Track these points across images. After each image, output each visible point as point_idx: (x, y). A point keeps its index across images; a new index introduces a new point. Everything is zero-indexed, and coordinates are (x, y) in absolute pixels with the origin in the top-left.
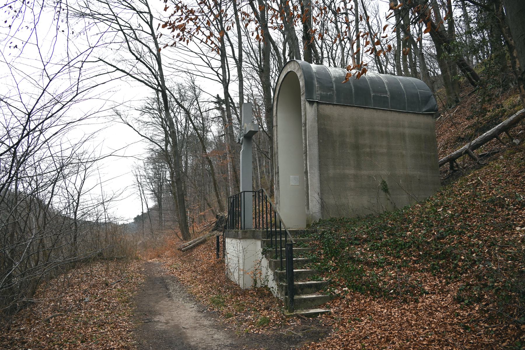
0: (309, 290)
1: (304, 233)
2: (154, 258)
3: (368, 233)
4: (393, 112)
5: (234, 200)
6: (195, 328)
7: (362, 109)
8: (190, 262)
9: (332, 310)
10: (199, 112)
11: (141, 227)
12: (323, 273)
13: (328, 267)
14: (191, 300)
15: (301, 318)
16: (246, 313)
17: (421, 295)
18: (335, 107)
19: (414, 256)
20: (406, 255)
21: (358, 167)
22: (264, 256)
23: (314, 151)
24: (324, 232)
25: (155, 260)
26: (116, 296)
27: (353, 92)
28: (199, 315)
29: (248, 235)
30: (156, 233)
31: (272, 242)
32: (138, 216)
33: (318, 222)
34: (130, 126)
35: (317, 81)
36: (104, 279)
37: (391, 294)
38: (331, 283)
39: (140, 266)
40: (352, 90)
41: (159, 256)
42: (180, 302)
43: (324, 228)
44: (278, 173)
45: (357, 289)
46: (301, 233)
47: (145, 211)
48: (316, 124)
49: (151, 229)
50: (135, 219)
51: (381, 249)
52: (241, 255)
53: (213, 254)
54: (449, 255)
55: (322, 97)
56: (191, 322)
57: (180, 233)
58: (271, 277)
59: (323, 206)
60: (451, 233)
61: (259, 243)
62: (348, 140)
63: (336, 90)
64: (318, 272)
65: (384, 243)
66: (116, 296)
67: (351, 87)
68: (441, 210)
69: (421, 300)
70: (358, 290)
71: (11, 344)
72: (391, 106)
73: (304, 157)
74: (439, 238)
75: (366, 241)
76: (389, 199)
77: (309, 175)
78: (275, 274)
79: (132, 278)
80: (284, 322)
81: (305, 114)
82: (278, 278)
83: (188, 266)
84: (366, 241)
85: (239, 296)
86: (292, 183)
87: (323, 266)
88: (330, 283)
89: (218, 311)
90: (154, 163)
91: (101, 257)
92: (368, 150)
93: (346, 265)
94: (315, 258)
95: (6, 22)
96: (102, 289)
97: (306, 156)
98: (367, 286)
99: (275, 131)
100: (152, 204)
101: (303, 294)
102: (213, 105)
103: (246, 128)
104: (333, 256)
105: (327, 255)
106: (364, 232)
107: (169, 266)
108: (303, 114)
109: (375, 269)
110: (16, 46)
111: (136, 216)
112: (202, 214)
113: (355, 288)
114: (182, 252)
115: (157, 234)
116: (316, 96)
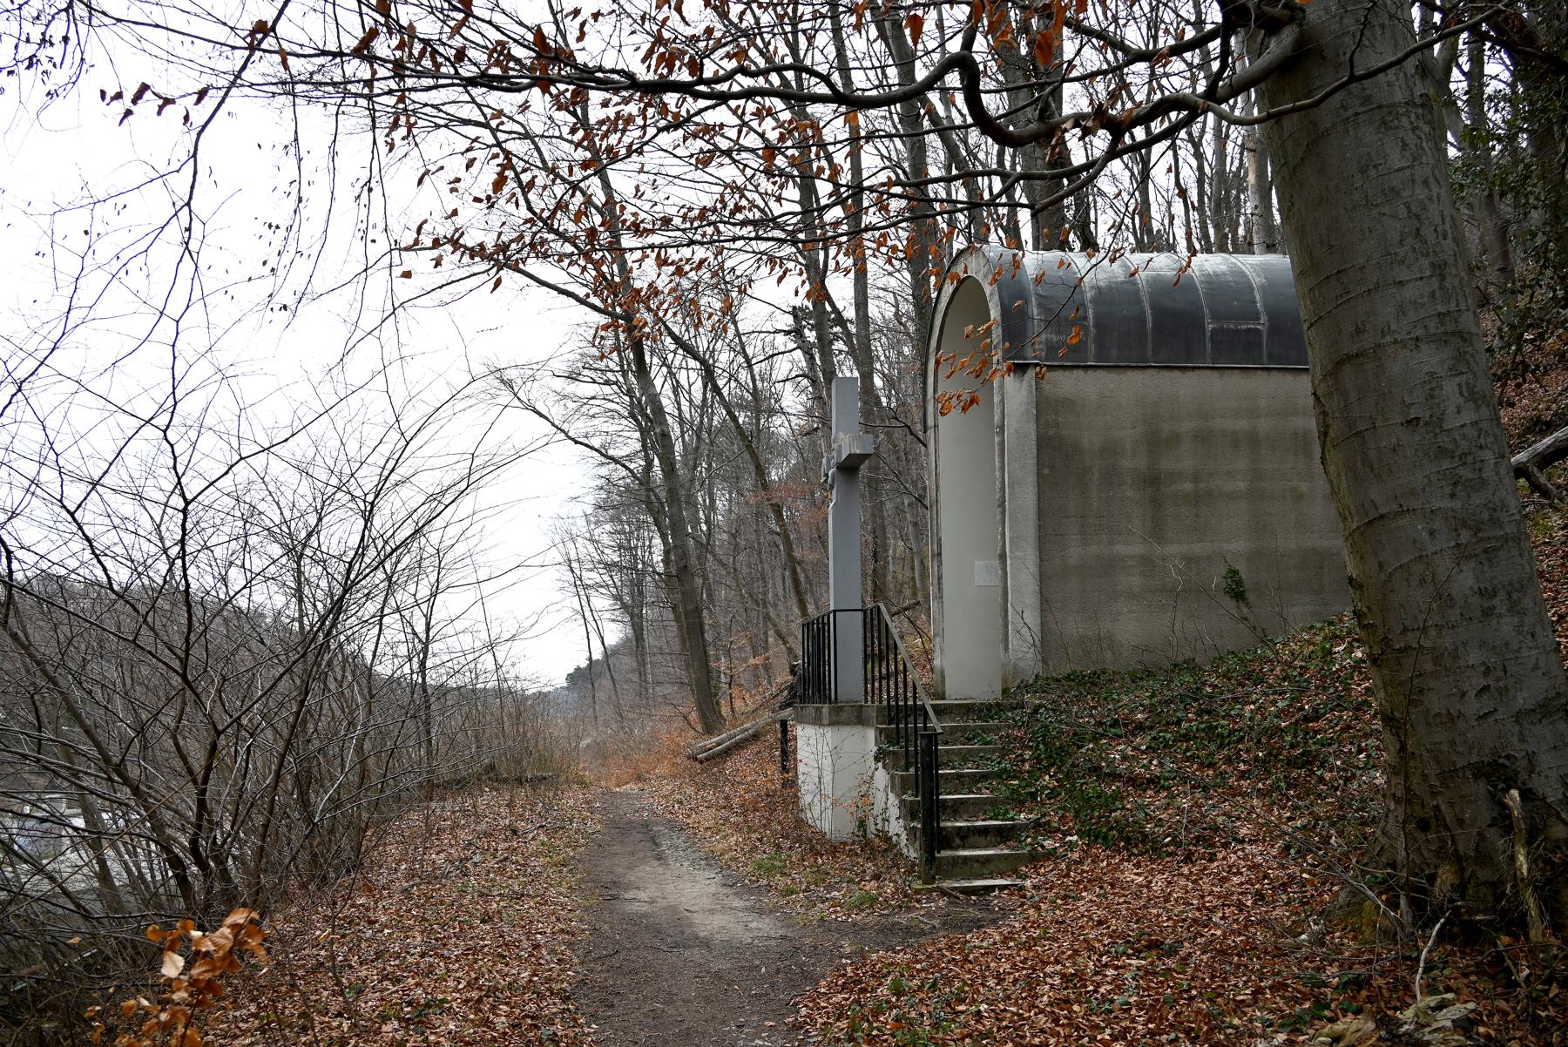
0: (981, 840)
1: (989, 710)
2: (627, 783)
3: (1150, 709)
4: (1274, 373)
5: (818, 628)
6: (712, 912)
7: (1177, 373)
8: (716, 787)
9: (1028, 883)
10: (741, 359)
11: (589, 700)
12: (1022, 803)
13: (1037, 791)
14: (711, 865)
15: (950, 896)
16: (829, 888)
17: (1226, 846)
18: (1091, 373)
19: (1244, 762)
20: (1228, 760)
21: (1157, 532)
22: (880, 764)
23: (1027, 498)
24: (1040, 706)
25: (632, 788)
26: (537, 854)
27: (1150, 325)
28: (726, 891)
29: (844, 716)
30: (631, 716)
31: (898, 733)
32: (578, 669)
33: (1031, 681)
34: (541, 415)
35: (1040, 305)
36: (507, 822)
37: (1167, 845)
38: (1039, 826)
39: (590, 797)
40: (1144, 321)
41: (639, 778)
42: (684, 869)
43: (1040, 698)
44: (939, 554)
45: (1097, 838)
46: (980, 710)
47: (598, 655)
48: (1032, 428)
49: (618, 707)
50: (570, 677)
51: (1173, 746)
52: (827, 763)
53: (773, 770)
54: (1315, 757)
55: (1051, 349)
56: (706, 902)
57: (694, 716)
58: (894, 812)
59: (1047, 642)
60: (1339, 705)
61: (871, 734)
62: (1127, 463)
63: (1097, 325)
64: (1007, 801)
65: (1183, 732)
66: (537, 854)
67: (1144, 312)
68: (1341, 648)
69: (1220, 856)
70: (1100, 840)
71: (349, 923)
72: (1270, 355)
73: (999, 517)
74: (1306, 719)
75: (1140, 727)
76: (1246, 619)
77: (1009, 562)
78: (903, 803)
79: (571, 821)
80: (907, 900)
81: (1002, 402)
82: (909, 812)
83: (710, 795)
84: (1140, 727)
85: (822, 855)
86: (980, 580)
87: (1024, 788)
88: (1037, 825)
89: (769, 885)
90: (615, 519)
91: (492, 776)
92: (1188, 487)
93: (1082, 784)
94: (1005, 769)
95: (265, 263)
96: (505, 841)
97: (1003, 513)
98: (1120, 833)
99: (932, 440)
100: (615, 633)
101: (964, 848)
102: (782, 342)
103: (840, 446)
104: (1053, 765)
105: (1039, 761)
106: (1141, 705)
107: (665, 796)
108: (996, 399)
109: (1150, 792)
110: (285, 307)
111: (572, 671)
112: (758, 661)
113: (1093, 836)
114: (698, 766)
115: (632, 720)
116: (1039, 339)
